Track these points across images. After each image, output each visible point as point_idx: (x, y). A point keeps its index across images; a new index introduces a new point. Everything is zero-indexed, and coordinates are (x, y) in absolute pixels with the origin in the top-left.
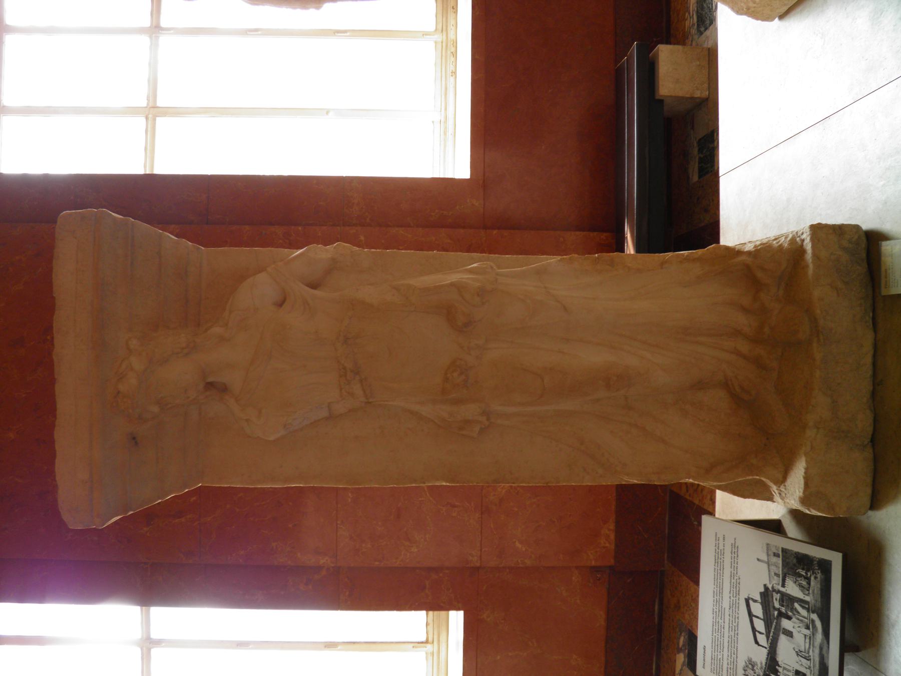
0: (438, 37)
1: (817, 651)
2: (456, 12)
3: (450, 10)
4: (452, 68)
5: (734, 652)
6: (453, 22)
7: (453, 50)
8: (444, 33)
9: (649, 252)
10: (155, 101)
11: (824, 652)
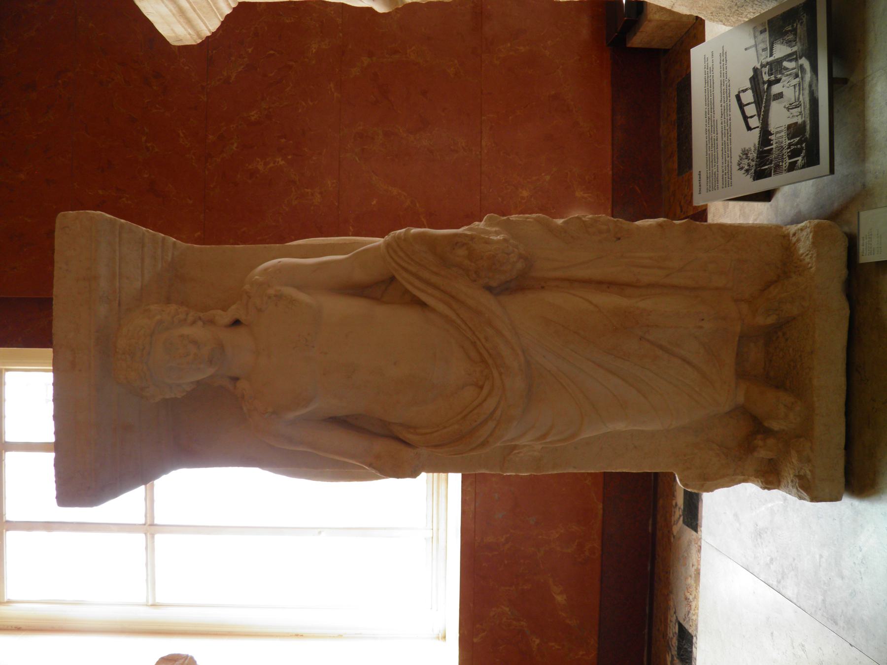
1: (807, 92)
5: (727, 146)
10: (153, 517)
11: (814, 88)
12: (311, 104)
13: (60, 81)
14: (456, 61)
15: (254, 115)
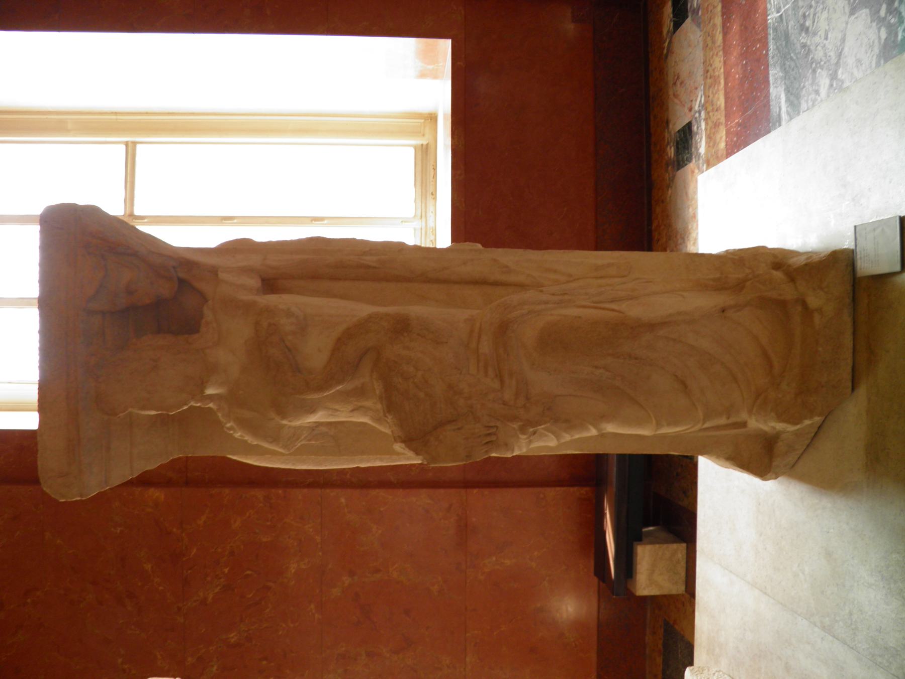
0: (417, 224)
2: (435, 199)
3: (429, 197)
4: (431, 190)
6: (432, 209)
7: (432, 238)
8: (424, 219)
9: (597, 248)
12: (292, 625)
13: (29, 601)
14: (440, 578)
15: (233, 637)
